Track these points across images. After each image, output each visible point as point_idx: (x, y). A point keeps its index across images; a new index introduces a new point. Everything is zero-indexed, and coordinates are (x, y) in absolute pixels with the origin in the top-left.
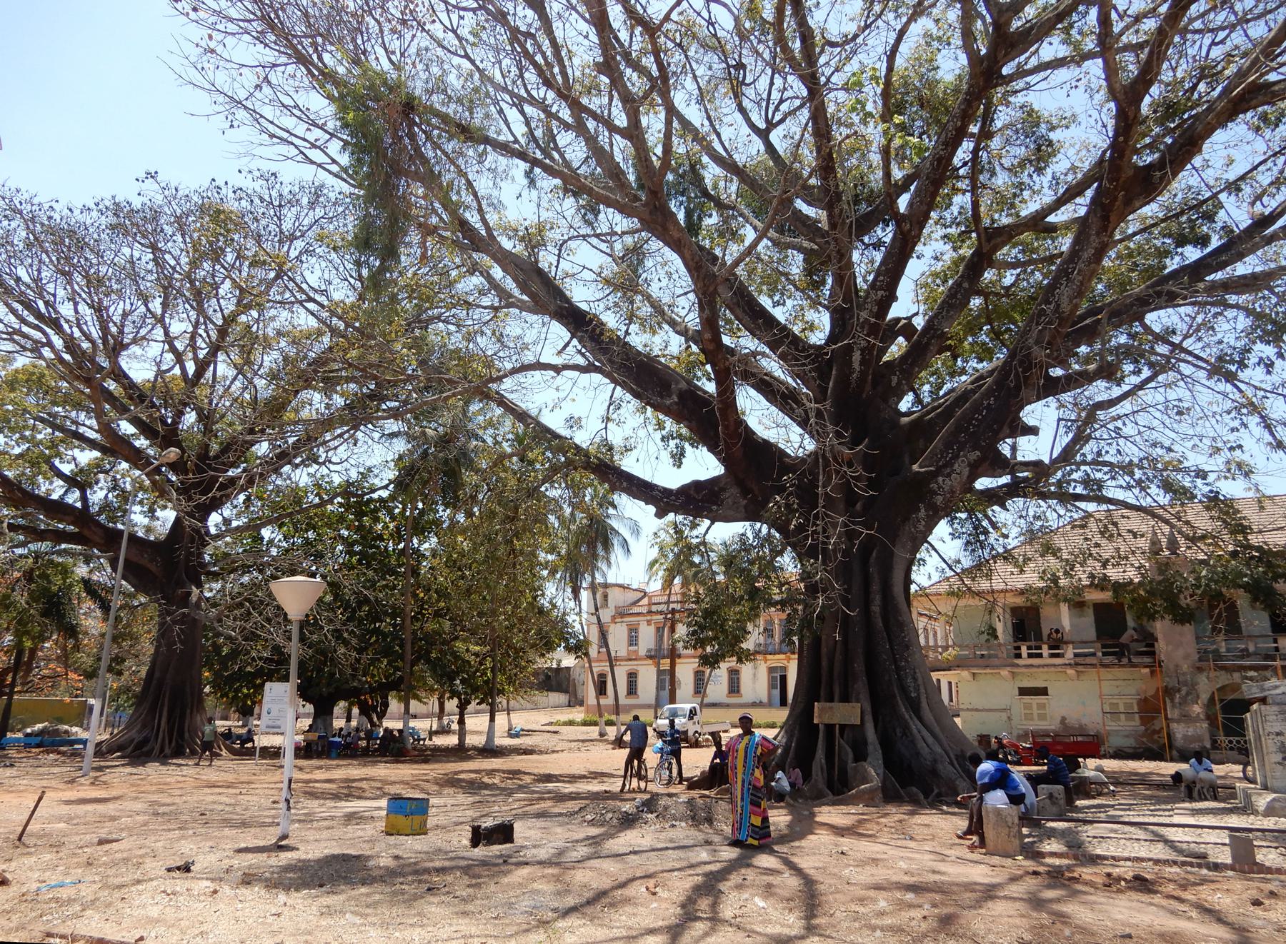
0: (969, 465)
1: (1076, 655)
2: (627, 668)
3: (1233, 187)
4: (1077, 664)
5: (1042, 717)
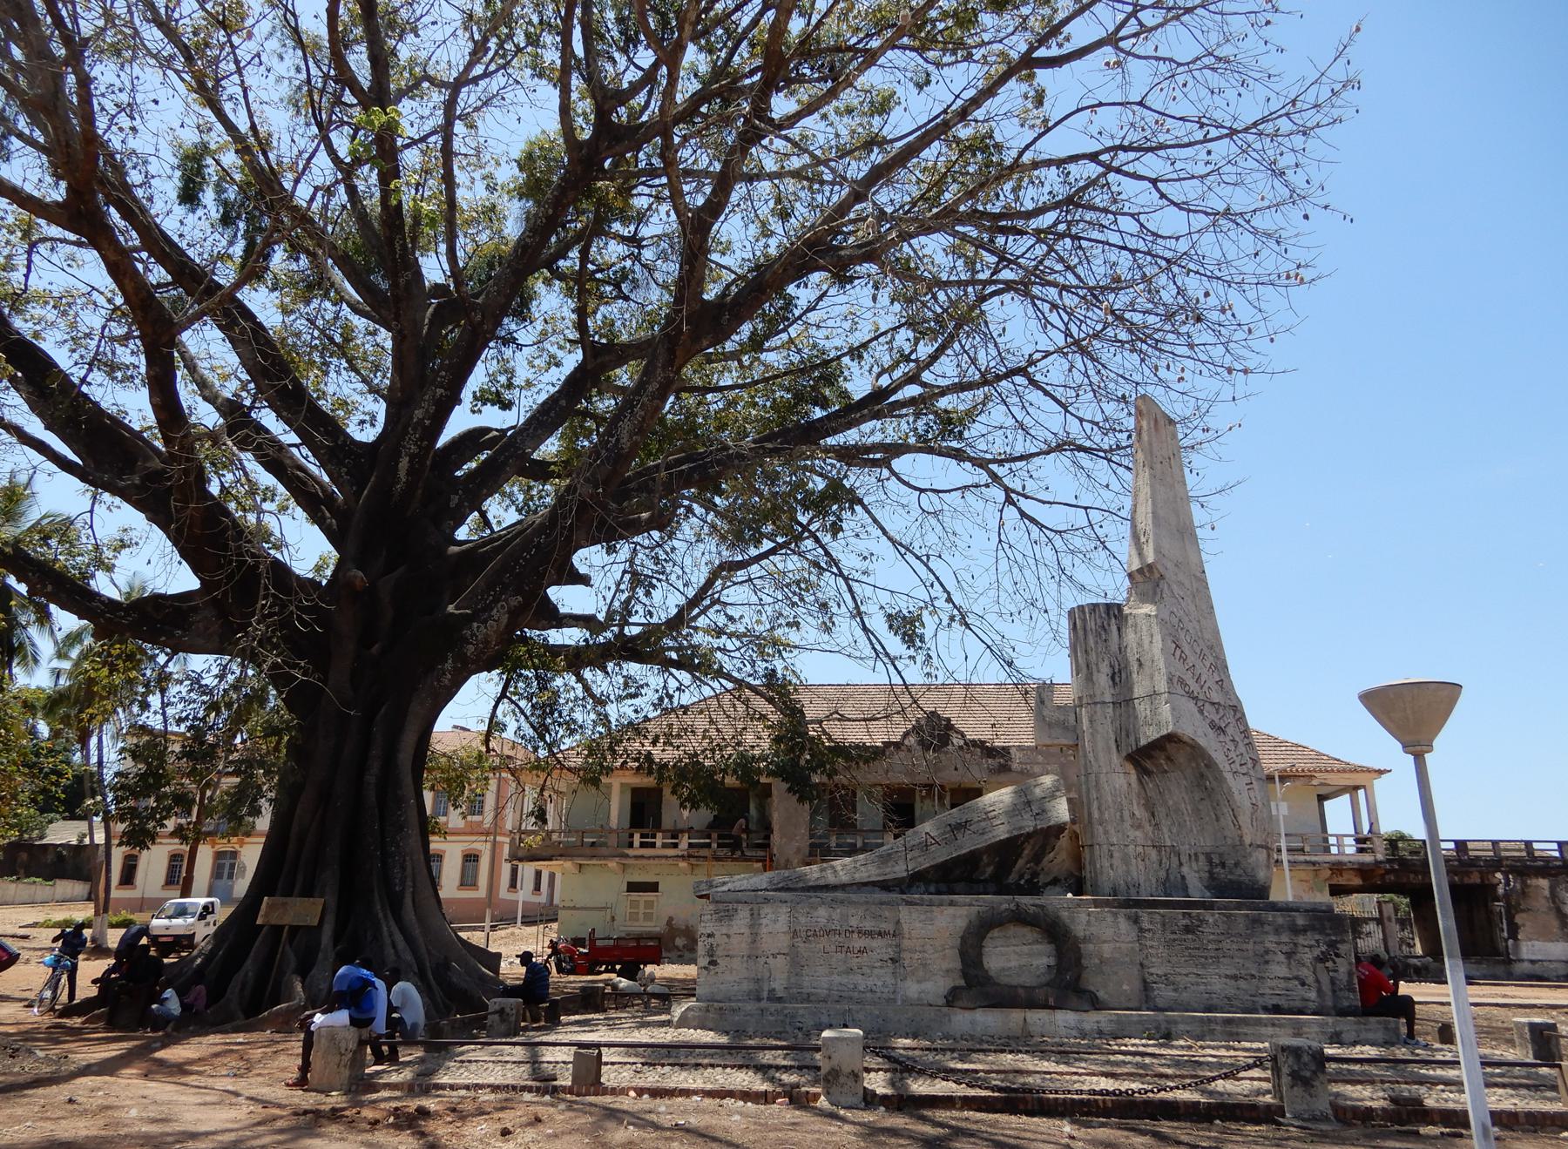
0: (509, 612)
1: (690, 845)
2: (465, 846)
3: (856, 352)
4: (690, 856)
5: (648, 917)
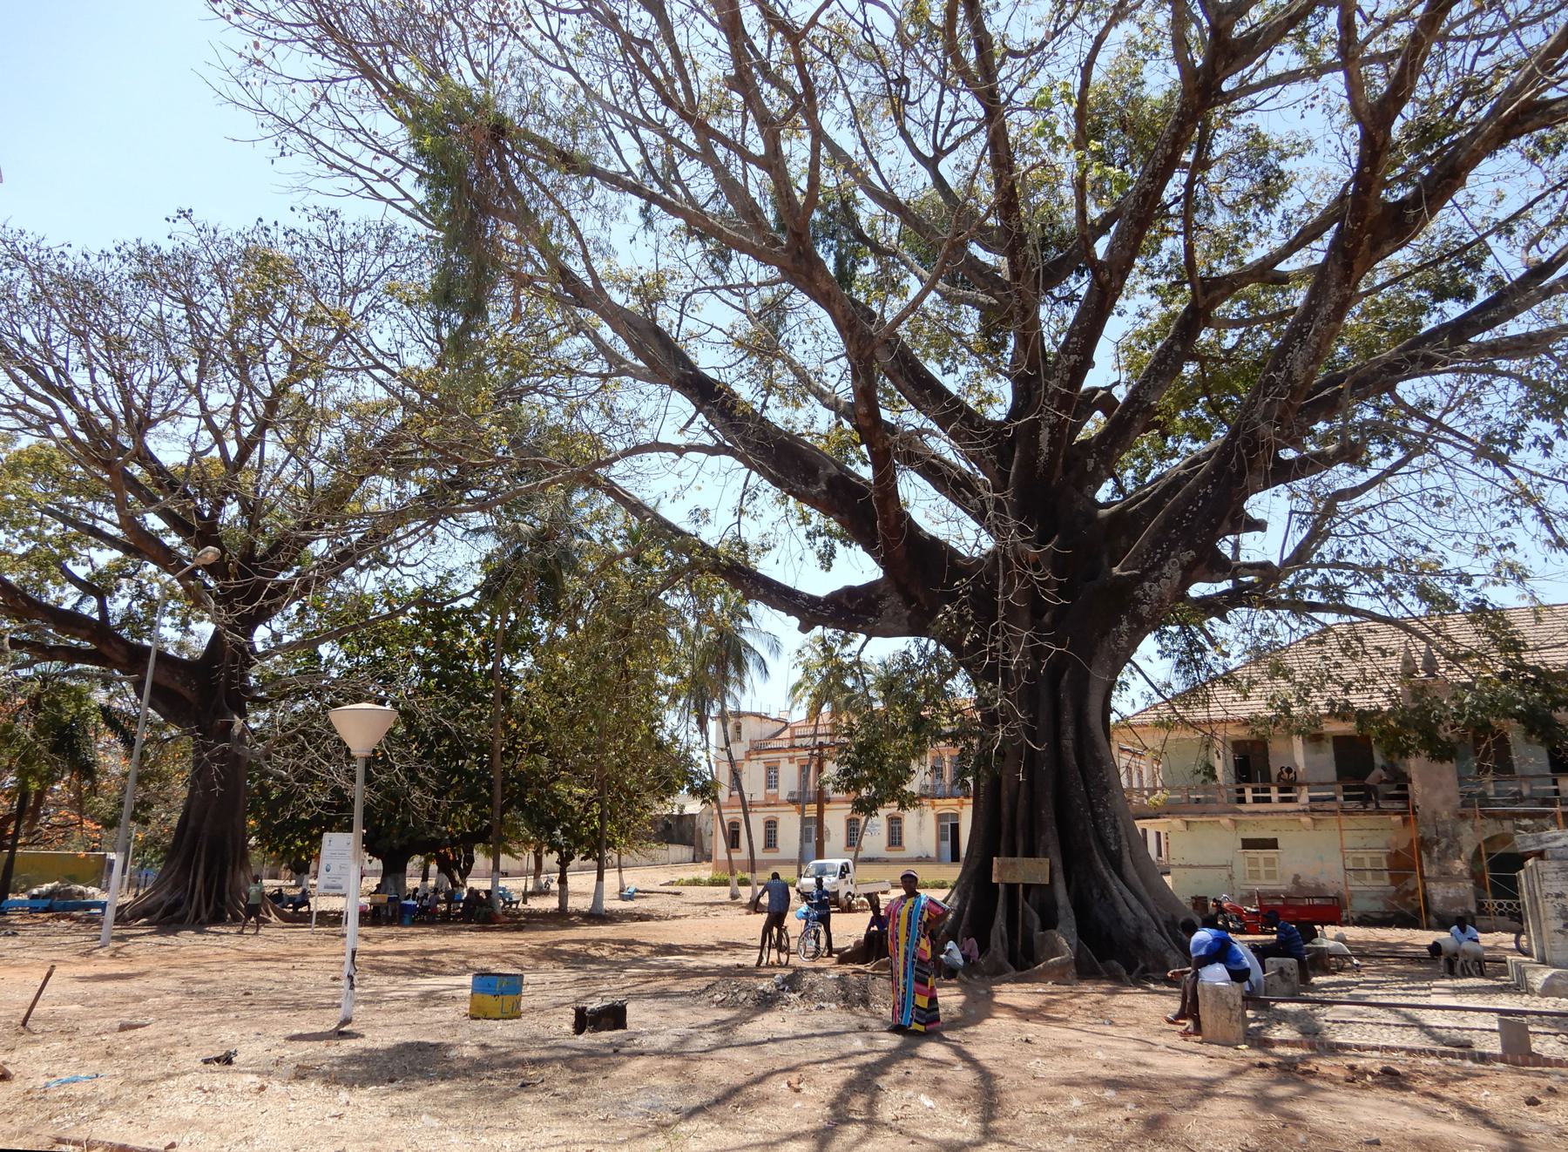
0: (1182, 567)
1: (1312, 799)
2: (765, 815)
3: (1504, 228)
4: (1313, 811)
5: (1271, 875)
